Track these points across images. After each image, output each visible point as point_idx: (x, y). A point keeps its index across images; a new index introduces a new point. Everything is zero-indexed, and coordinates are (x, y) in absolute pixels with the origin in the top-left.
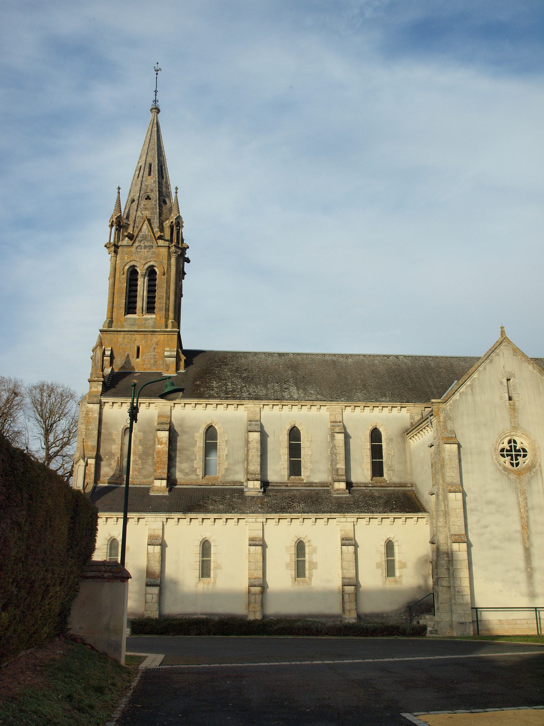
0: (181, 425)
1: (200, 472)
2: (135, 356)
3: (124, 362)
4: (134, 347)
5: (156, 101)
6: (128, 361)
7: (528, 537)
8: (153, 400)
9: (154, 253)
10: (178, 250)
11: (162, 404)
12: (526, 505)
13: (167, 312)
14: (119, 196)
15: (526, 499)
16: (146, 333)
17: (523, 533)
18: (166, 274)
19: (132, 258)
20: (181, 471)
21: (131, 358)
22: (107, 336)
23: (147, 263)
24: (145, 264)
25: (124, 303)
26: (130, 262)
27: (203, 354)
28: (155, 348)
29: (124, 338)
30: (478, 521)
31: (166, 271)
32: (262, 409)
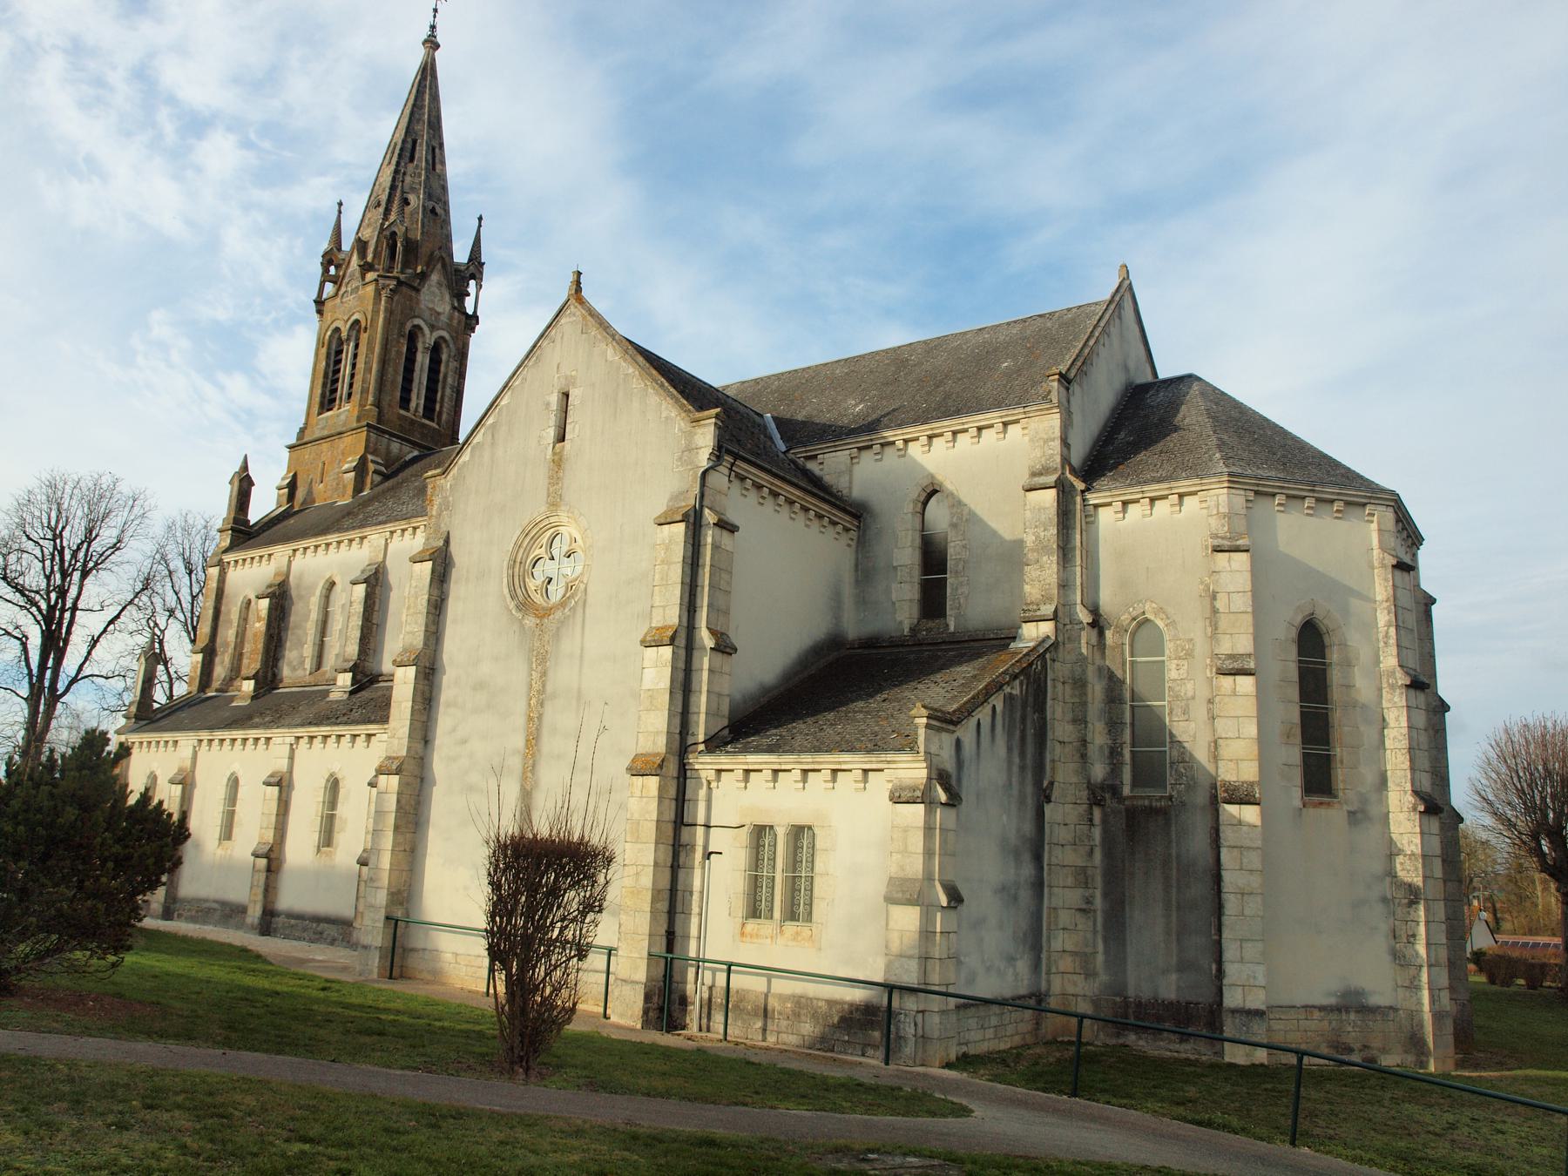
0: (298, 586)
1: (308, 665)
5: (433, 27)
7: (534, 766)
8: (271, 550)
12: (542, 691)
15: (544, 674)
17: (525, 757)
20: (289, 664)
22: (307, 453)
30: (454, 730)
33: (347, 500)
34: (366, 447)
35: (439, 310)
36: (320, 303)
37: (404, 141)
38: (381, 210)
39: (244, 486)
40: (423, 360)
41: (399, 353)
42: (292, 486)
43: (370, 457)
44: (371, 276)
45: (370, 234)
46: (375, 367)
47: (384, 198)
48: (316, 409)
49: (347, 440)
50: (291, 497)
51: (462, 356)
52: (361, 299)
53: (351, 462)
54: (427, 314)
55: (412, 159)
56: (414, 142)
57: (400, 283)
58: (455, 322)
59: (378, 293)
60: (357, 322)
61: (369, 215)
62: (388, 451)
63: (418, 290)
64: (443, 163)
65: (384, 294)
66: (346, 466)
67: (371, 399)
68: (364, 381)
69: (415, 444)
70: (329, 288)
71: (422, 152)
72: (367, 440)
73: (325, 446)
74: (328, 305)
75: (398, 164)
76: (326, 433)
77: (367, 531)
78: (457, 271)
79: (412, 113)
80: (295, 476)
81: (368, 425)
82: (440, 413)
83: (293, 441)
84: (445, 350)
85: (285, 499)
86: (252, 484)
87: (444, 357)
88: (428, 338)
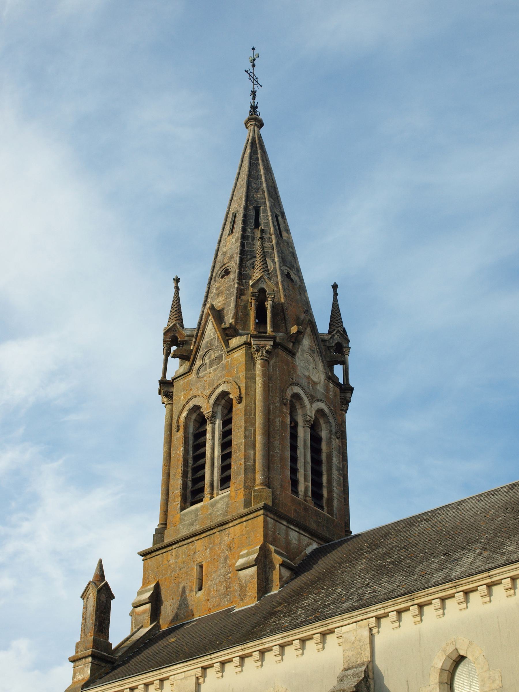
2: (195, 587)
3: (176, 606)
4: (192, 569)
5: (254, 108)
6: (183, 603)
8: (165, 672)
9: (224, 367)
10: (263, 343)
11: (181, 676)
13: (250, 475)
14: (335, 300)
16: (211, 532)
18: (244, 400)
19: (191, 394)
21: (187, 592)
22: (172, 558)
23: (213, 392)
24: (211, 395)
25: (179, 486)
26: (187, 403)
27: (361, 537)
28: (226, 558)
29: (177, 557)
31: (243, 392)
32: (375, 631)
33: (251, 602)
34: (265, 535)
35: (316, 380)
36: (166, 387)
37: (246, 209)
38: (233, 276)
39: (102, 596)
40: (303, 434)
41: (283, 423)
42: (156, 600)
43: (272, 548)
44: (234, 342)
45: (226, 302)
46: (259, 439)
47: (234, 265)
48: (176, 502)
49: (234, 531)
50: (155, 614)
51: (341, 433)
52: (228, 368)
53: (249, 554)
54: (304, 382)
55: (257, 224)
56: (257, 210)
57: (276, 345)
58: (331, 393)
59: (250, 360)
60: (225, 394)
61: (215, 286)
62: (288, 543)
63: (293, 354)
64: (288, 231)
65: (258, 357)
66: (240, 562)
67: (259, 477)
68: (246, 458)
69: (314, 535)
70: (175, 366)
71: (267, 217)
72: (266, 526)
73: (199, 544)
74: (179, 384)
75: (244, 230)
76: (197, 528)
77: (333, 623)
78: (324, 341)
79: (249, 184)
80: (157, 588)
81: (266, 508)
82: (330, 500)
83: (149, 544)
84: (323, 426)
85: (147, 617)
86: (112, 597)
87: (324, 434)
88: (310, 409)
